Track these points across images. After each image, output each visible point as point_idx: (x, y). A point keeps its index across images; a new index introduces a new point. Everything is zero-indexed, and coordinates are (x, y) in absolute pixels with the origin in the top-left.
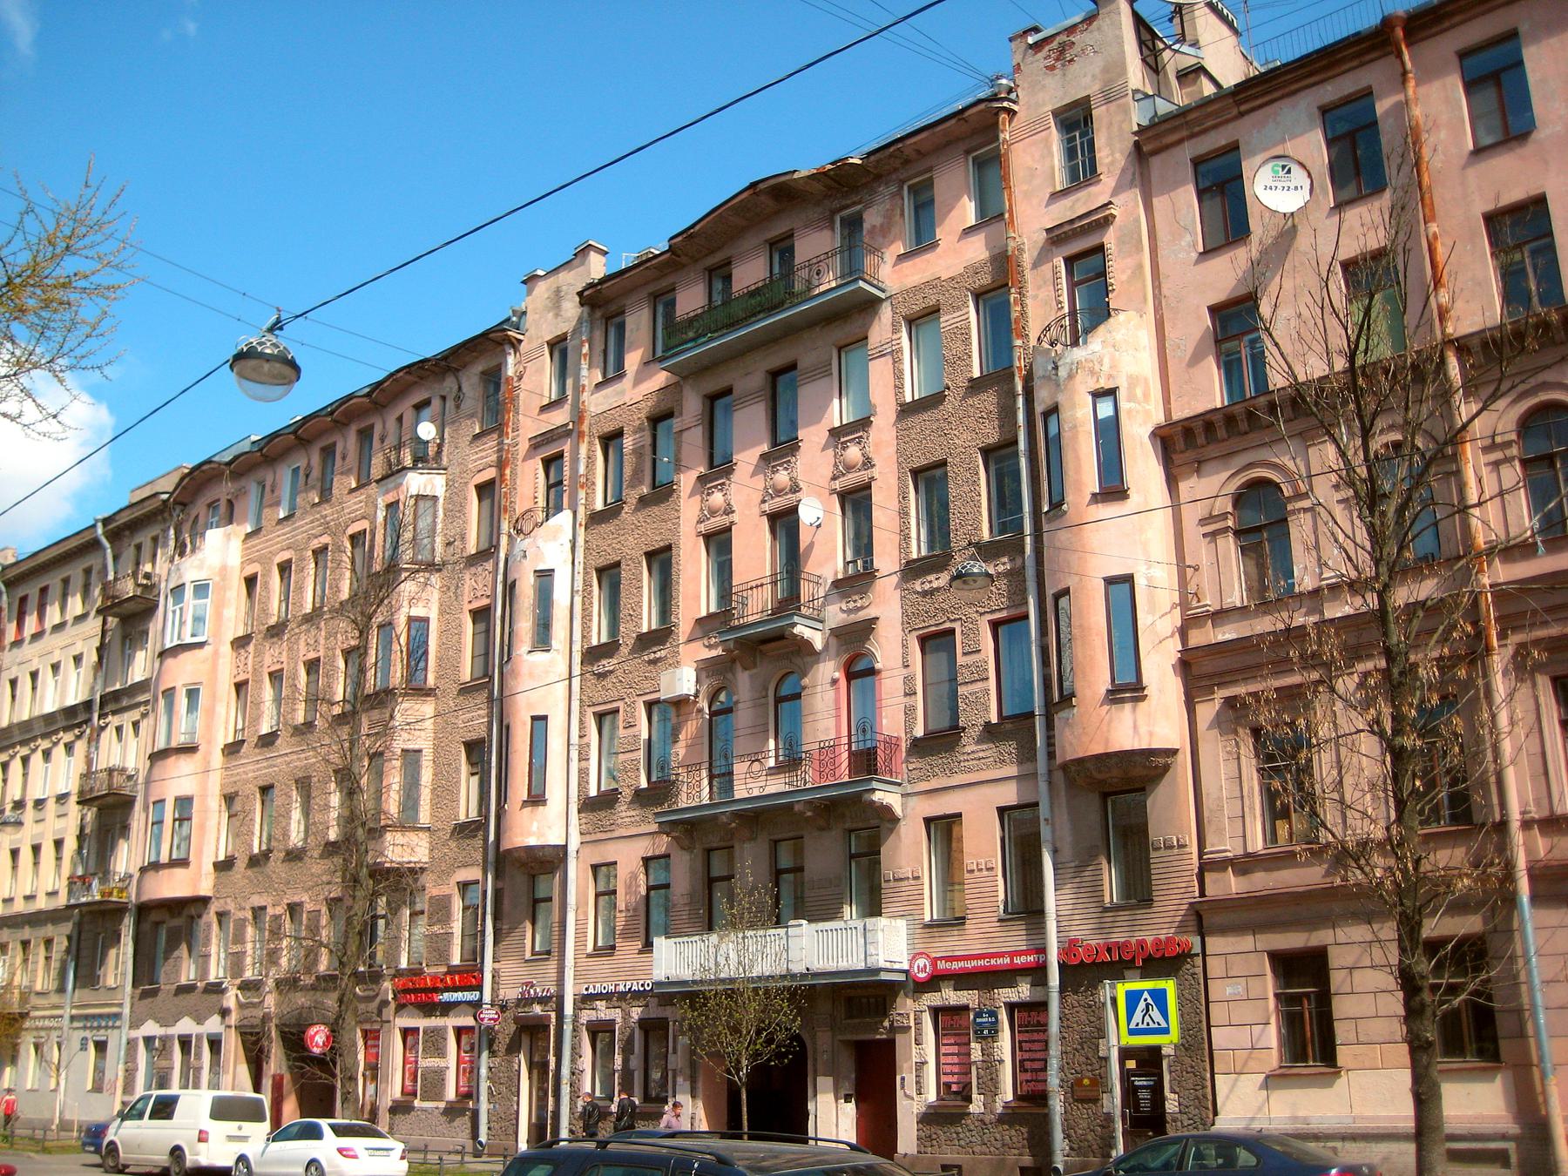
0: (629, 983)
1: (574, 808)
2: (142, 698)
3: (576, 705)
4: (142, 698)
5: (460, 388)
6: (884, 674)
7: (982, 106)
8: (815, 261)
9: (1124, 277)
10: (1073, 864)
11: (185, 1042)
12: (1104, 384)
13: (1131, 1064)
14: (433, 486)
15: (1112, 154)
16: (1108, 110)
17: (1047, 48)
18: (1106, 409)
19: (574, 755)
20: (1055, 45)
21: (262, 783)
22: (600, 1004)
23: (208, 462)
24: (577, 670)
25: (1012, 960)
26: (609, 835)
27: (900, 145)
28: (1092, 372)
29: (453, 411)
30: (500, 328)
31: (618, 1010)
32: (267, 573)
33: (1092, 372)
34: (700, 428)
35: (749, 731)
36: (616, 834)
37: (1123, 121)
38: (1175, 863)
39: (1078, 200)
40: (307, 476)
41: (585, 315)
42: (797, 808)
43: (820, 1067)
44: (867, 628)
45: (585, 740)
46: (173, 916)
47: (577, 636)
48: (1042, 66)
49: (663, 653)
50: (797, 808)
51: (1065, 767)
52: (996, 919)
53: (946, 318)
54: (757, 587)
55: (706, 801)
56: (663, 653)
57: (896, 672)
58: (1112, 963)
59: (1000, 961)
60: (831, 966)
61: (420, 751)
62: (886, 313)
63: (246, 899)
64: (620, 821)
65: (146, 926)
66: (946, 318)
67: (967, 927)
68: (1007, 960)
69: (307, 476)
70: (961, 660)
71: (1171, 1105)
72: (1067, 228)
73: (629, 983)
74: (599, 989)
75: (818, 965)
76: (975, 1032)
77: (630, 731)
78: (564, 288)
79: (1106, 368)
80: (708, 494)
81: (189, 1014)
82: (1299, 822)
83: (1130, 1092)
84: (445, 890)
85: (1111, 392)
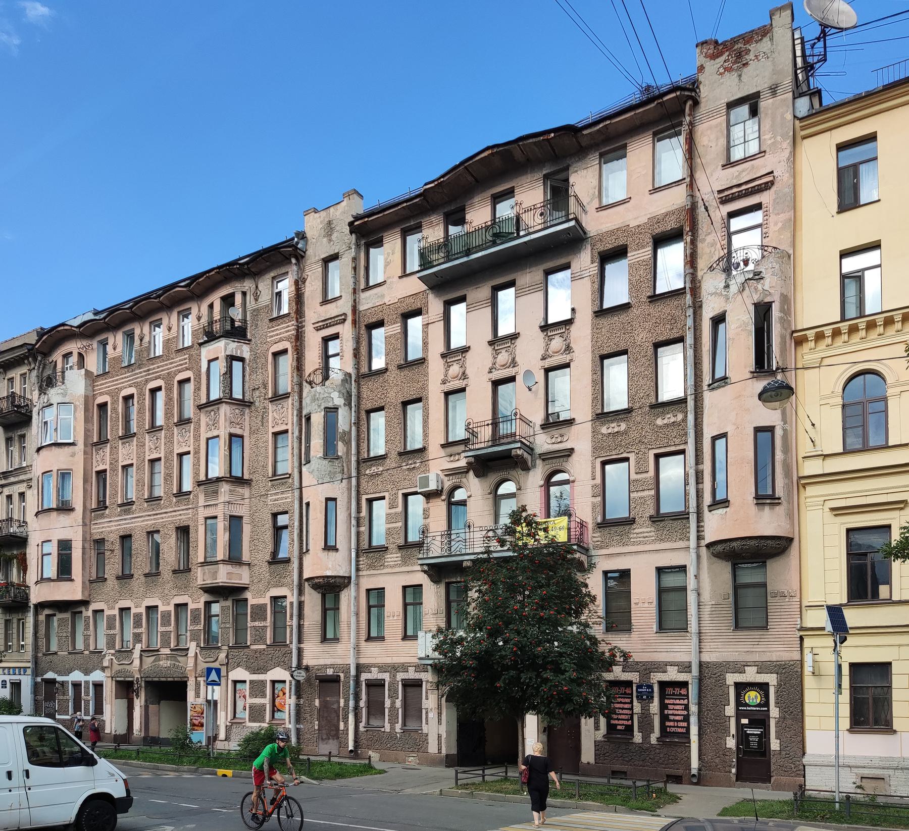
2: (22, 477)
4: (22, 477)
5: (257, 287)
9: (777, 228)
10: (710, 603)
11: (77, 686)
13: (745, 721)
14: (242, 352)
15: (774, 137)
19: (354, 522)
21: (122, 534)
23: (63, 325)
26: (379, 572)
27: (608, 122)
29: (253, 302)
30: (289, 243)
31: (388, 674)
32: (115, 402)
34: (442, 322)
36: (383, 571)
38: (786, 607)
40: (141, 340)
41: (354, 241)
45: (700, 467)
46: (61, 612)
50: (464, 564)
53: (633, 254)
55: (366, 457)
61: (241, 517)
63: (116, 602)
64: (386, 564)
65: (42, 618)
66: (633, 254)
67: (632, 636)
69: (141, 340)
71: (775, 745)
72: (735, 190)
76: (637, 697)
80: (449, 366)
81: (80, 669)
82: (46, 374)
83: (742, 737)
84: (261, 601)
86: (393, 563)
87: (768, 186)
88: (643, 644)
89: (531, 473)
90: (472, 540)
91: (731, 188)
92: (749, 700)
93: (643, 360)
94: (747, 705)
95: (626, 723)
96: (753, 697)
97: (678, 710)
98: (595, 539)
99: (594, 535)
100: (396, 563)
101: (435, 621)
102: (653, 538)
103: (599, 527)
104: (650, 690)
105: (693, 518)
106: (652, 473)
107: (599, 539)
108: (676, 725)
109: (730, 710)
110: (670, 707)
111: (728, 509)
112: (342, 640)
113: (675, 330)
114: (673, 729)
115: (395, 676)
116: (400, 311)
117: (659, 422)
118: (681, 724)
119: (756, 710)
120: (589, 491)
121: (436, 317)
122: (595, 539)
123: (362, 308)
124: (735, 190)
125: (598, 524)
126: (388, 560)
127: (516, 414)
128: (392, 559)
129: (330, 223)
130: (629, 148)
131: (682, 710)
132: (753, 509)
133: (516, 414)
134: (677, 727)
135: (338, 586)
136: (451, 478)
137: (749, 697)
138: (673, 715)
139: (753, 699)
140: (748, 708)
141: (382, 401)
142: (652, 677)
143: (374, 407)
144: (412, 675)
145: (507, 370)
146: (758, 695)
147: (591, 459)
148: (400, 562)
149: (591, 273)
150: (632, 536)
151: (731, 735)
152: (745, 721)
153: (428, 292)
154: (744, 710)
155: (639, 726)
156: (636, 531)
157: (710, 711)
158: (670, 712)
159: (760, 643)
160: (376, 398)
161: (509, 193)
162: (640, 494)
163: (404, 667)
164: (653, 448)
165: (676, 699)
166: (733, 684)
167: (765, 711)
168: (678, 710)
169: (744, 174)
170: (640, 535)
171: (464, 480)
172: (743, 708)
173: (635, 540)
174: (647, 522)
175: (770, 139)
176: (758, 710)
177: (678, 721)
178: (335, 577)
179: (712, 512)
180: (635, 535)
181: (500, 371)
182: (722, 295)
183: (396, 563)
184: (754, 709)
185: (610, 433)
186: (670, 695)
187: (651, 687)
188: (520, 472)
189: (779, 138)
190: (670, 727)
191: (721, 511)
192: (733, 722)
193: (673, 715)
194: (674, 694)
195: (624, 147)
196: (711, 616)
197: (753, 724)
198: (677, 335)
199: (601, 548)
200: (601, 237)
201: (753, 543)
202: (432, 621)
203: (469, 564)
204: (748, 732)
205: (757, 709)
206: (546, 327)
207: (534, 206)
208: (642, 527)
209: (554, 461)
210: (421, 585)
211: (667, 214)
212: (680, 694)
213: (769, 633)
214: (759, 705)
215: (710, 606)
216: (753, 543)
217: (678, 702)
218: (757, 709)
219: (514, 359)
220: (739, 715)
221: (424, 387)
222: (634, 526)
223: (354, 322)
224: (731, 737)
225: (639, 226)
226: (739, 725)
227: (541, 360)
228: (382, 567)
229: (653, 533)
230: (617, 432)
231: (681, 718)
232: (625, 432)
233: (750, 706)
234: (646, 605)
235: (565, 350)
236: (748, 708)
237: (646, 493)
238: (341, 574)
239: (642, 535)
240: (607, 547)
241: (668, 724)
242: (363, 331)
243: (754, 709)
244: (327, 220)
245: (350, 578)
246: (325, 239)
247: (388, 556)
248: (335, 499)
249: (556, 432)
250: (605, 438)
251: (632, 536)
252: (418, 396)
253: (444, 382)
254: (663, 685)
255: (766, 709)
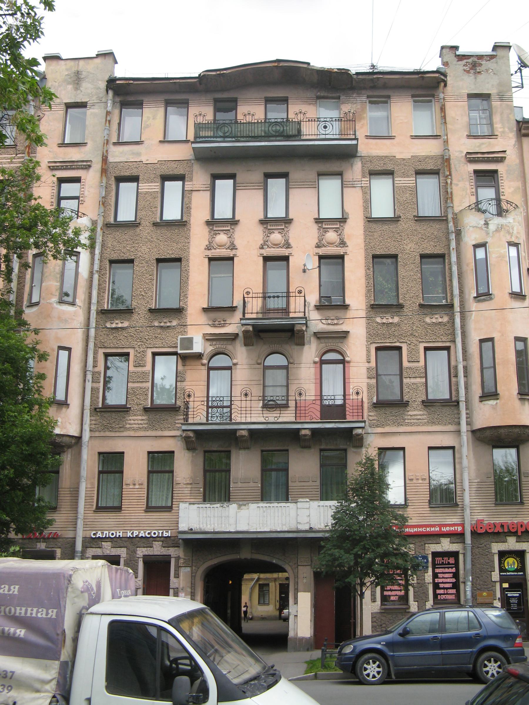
0: (161, 532)
1: (87, 413)
3: (91, 345)
6: (352, 364)
7: (437, 75)
8: (322, 120)
10: (476, 481)
12: (513, 239)
13: (506, 585)
16: (501, 105)
17: (465, 61)
18: (480, 253)
19: (89, 377)
20: (470, 60)
22: (107, 545)
24: (93, 324)
25: (440, 529)
26: (118, 434)
28: (509, 232)
31: (124, 550)
33: (509, 232)
35: (245, 383)
37: (510, 114)
39: (483, 144)
42: (355, 432)
43: (300, 586)
44: (344, 335)
47: (94, 300)
48: (462, 68)
49: (126, 324)
50: (303, 432)
51: (473, 432)
52: (525, 505)
54: (274, 297)
56: (126, 324)
57: (361, 365)
58: (102, 538)
59: (433, 529)
60: (209, 528)
62: (358, 166)
64: (128, 426)
67: (408, 510)
68: (437, 529)
70: (405, 364)
72: (479, 156)
73: (105, 532)
74: (106, 533)
75: (195, 526)
77: (140, 369)
78: (84, 73)
79: (515, 232)
80: (216, 234)
85: (483, 245)
86: (137, 426)
87: (501, 160)
88: (418, 518)
89: (306, 347)
90: (245, 409)
91: (477, 153)
92: (508, 565)
93: (412, 266)
94: (506, 571)
95: (399, 593)
96: (511, 563)
97: (447, 578)
98: (371, 418)
99: (370, 414)
100: (141, 426)
101: (189, 492)
102: (426, 421)
103: (375, 407)
104: (425, 560)
105: (462, 405)
106: (422, 363)
107: (375, 418)
108: (446, 592)
109: (496, 576)
110: (440, 575)
111: (498, 401)
112: (62, 509)
113: (438, 248)
114: (443, 597)
115: (135, 552)
116: (159, 173)
117: (428, 320)
118: (450, 591)
119: (514, 575)
120: (363, 371)
121: (202, 186)
122: (371, 418)
123: (111, 159)
124: (479, 156)
125: (374, 404)
126: (129, 422)
127: (300, 292)
128: (136, 422)
129: (78, 73)
130: (393, 100)
131: (451, 578)
132: (517, 403)
133: (300, 292)
134: (447, 594)
135: (63, 447)
136: (214, 343)
137: (508, 563)
138: (443, 583)
139: (511, 566)
140: (508, 574)
141: (132, 254)
142: (426, 548)
143: (120, 258)
144: (157, 549)
145: (280, 249)
146: (515, 561)
147: (366, 343)
148: (146, 426)
149: (363, 185)
150: (406, 417)
151: (497, 598)
152: (506, 585)
153: (193, 162)
154: (504, 575)
155: (414, 595)
156: (410, 413)
157: (478, 577)
158: (440, 580)
159: (518, 516)
160: (124, 250)
161: (285, 100)
162: (413, 380)
163: (147, 541)
164: (423, 342)
165: (445, 568)
166: (497, 552)
167: (521, 575)
168: (447, 578)
169: (484, 146)
170: (413, 417)
171: (230, 347)
172: (503, 574)
173: (409, 421)
174: (420, 406)
175: (501, 128)
176: (516, 575)
177: (447, 588)
178: (63, 435)
179: (483, 402)
180: (409, 417)
181: (272, 249)
182: (482, 229)
183: (141, 426)
184: (513, 573)
185: (384, 323)
186: (440, 565)
187: (425, 557)
188: (296, 347)
189: (506, 130)
190: (441, 594)
191: (492, 402)
192: (498, 585)
193: (443, 583)
194: (443, 564)
195: (389, 97)
196: (477, 492)
197: (513, 587)
198: (440, 252)
199: (377, 426)
200: (371, 159)
201: (517, 430)
202: (186, 492)
203: (308, 432)
204: (509, 595)
205: (515, 573)
206: (319, 221)
207: (318, 118)
208: (415, 409)
209: (330, 340)
210: (173, 452)
211: (427, 157)
212: (449, 564)
213: (524, 507)
214: (516, 570)
215: (476, 484)
216: (517, 430)
217: (446, 570)
218: (515, 573)
219: (288, 240)
220: (503, 580)
221: (186, 248)
222: (409, 408)
223: (104, 171)
224: (497, 601)
225: (404, 159)
226: (503, 590)
227: (316, 247)
228: (122, 429)
229: (425, 416)
230: (391, 323)
231: (450, 585)
232: (398, 325)
233: (509, 571)
234: (420, 481)
235: (340, 244)
236: (508, 574)
237: (418, 380)
238: (71, 434)
239: (416, 417)
240: (383, 426)
241: (438, 591)
242: (113, 182)
243: (513, 573)
244: (74, 69)
245: (79, 439)
246: (70, 87)
247: (130, 418)
248: (491, 340)
249: (332, 313)
250: (379, 327)
251: (406, 417)
252: (177, 256)
253: (208, 248)
254: (435, 555)
255: (522, 573)
